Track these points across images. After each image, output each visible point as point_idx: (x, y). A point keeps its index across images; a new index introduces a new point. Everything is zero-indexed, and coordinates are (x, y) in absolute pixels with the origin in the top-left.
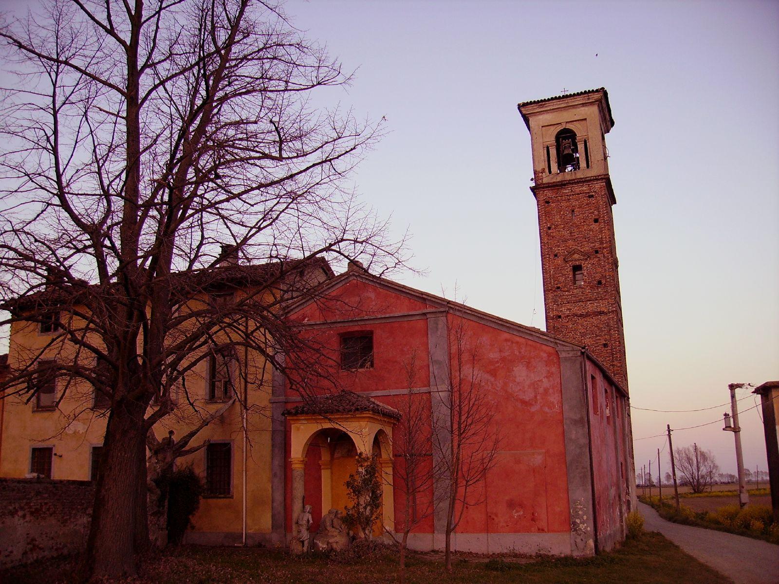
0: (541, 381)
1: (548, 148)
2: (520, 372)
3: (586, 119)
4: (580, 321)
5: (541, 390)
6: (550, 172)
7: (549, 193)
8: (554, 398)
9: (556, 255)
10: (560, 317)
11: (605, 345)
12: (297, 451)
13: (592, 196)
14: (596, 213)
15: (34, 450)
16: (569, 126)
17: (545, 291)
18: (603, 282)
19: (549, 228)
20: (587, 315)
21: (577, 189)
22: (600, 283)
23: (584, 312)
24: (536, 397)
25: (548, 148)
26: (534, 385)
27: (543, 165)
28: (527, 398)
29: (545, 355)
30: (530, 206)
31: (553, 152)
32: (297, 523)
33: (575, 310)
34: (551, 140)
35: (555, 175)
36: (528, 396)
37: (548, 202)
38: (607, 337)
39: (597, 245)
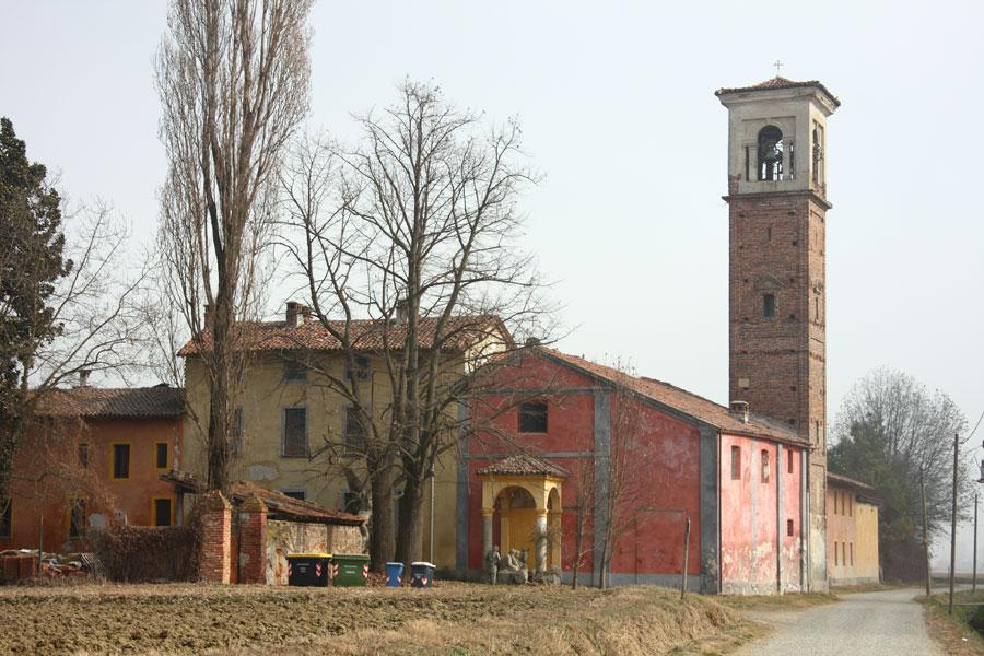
0: (684, 453)
1: (747, 148)
2: (669, 445)
3: (794, 117)
4: (769, 358)
5: (684, 460)
6: (748, 179)
7: (744, 207)
8: (694, 468)
9: (746, 281)
10: (745, 352)
11: (794, 389)
12: (488, 503)
13: (792, 214)
14: (795, 234)
15: (127, 477)
16: (774, 123)
17: (732, 321)
18: (797, 316)
19: (742, 248)
20: (776, 353)
21: (777, 203)
22: (792, 317)
23: (772, 349)
24: (679, 466)
25: (747, 148)
26: (679, 457)
27: (741, 169)
28: (673, 466)
29: (689, 432)
30: (725, 208)
31: (753, 154)
32: (488, 559)
33: (763, 346)
34: (753, 138)
35: (751, 187)
36: (673, 465)
37: (742, 216)
38: (796, 380)
39: (793, 273)
